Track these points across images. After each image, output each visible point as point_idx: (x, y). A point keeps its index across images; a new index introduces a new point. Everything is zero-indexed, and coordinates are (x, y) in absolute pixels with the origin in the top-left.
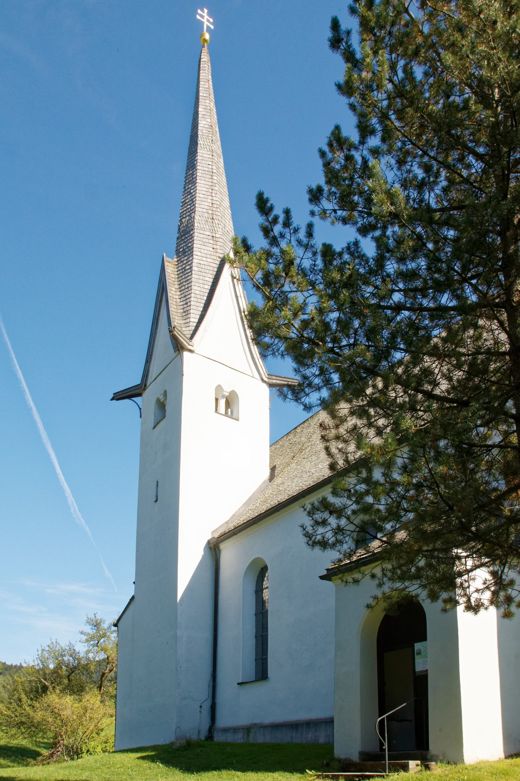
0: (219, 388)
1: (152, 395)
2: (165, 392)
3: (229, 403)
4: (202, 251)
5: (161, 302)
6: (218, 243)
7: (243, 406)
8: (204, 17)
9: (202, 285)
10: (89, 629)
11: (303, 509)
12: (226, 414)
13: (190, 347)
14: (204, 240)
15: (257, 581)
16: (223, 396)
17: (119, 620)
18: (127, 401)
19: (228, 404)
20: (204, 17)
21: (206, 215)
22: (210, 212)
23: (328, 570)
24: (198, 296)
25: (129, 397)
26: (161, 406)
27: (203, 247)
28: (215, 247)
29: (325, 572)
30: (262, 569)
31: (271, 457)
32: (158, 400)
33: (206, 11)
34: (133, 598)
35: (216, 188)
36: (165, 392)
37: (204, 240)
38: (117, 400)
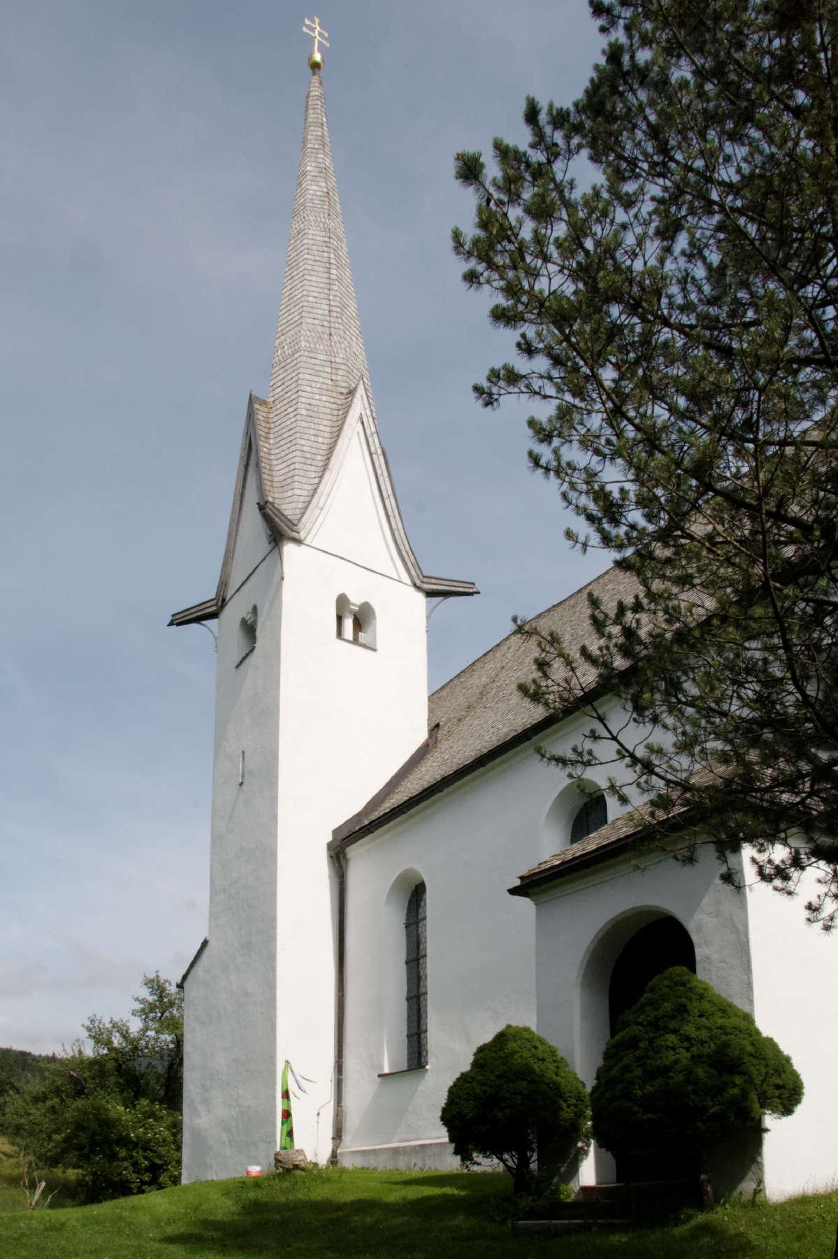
0: (342, 601)
1: (231, 616)
2: (255, 609)
3: (356, 620)
4: (314, 384)
5: (246, 467)
6: (340, 372)
7: (382, 626)
8: (315, 30)
9: (313, 438)
10: (145, 993)
11: (540, 471)
12: (355, 641)
13: (295, 535)
14: (317, 368)
15: (409, 909)
16: (351, 611)
17: (185, 977)
18: (194, 626)
19: (359, 625)
20: (315, 30)
21: (320, 329)
22: (326, 324)
23: (522, 878)
24: (308, 455)
25: (198, 620)
26: (249, 629)
27: (315, 378)
28: (334, 377)
29: (518, 883)
30: (417, 887)
31: (431, 711)
32: (244, 622)
33: (317, 21)
34: (205, 943)
35: (335, 288)
36: (255, 609)
37: (317, 368)
38: (178, 624)
